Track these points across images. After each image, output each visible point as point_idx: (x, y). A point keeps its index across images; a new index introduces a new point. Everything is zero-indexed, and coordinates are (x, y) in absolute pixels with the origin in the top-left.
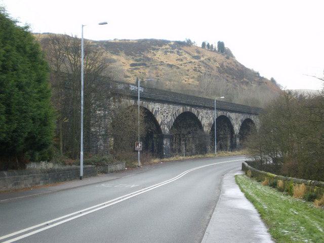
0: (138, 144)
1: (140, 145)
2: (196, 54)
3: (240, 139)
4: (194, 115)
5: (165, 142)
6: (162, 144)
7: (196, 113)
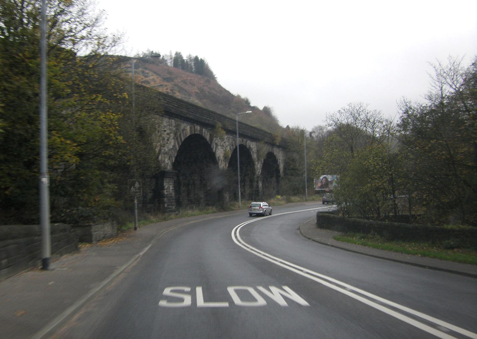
0: (133, 184)
1: (137, 185)
2: (168, 76)
3: (263, 182)
4: (203, 138)
5: (166, 185)
6: (163, 188)
7: (208, 138)
